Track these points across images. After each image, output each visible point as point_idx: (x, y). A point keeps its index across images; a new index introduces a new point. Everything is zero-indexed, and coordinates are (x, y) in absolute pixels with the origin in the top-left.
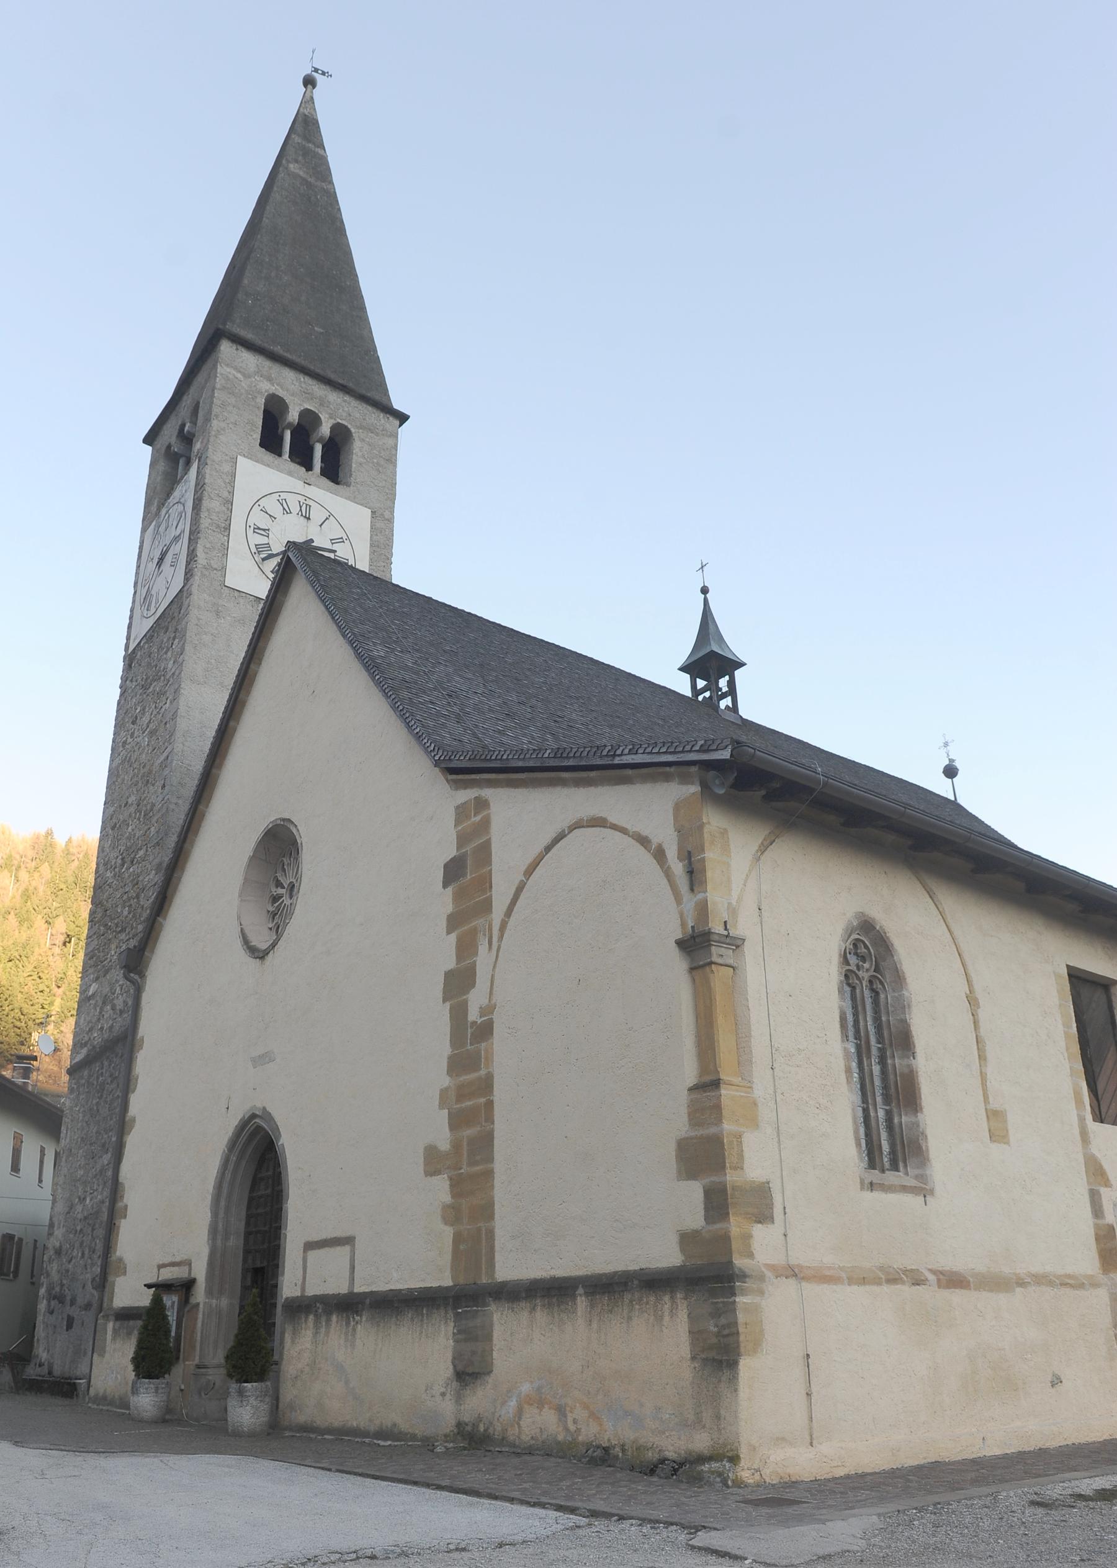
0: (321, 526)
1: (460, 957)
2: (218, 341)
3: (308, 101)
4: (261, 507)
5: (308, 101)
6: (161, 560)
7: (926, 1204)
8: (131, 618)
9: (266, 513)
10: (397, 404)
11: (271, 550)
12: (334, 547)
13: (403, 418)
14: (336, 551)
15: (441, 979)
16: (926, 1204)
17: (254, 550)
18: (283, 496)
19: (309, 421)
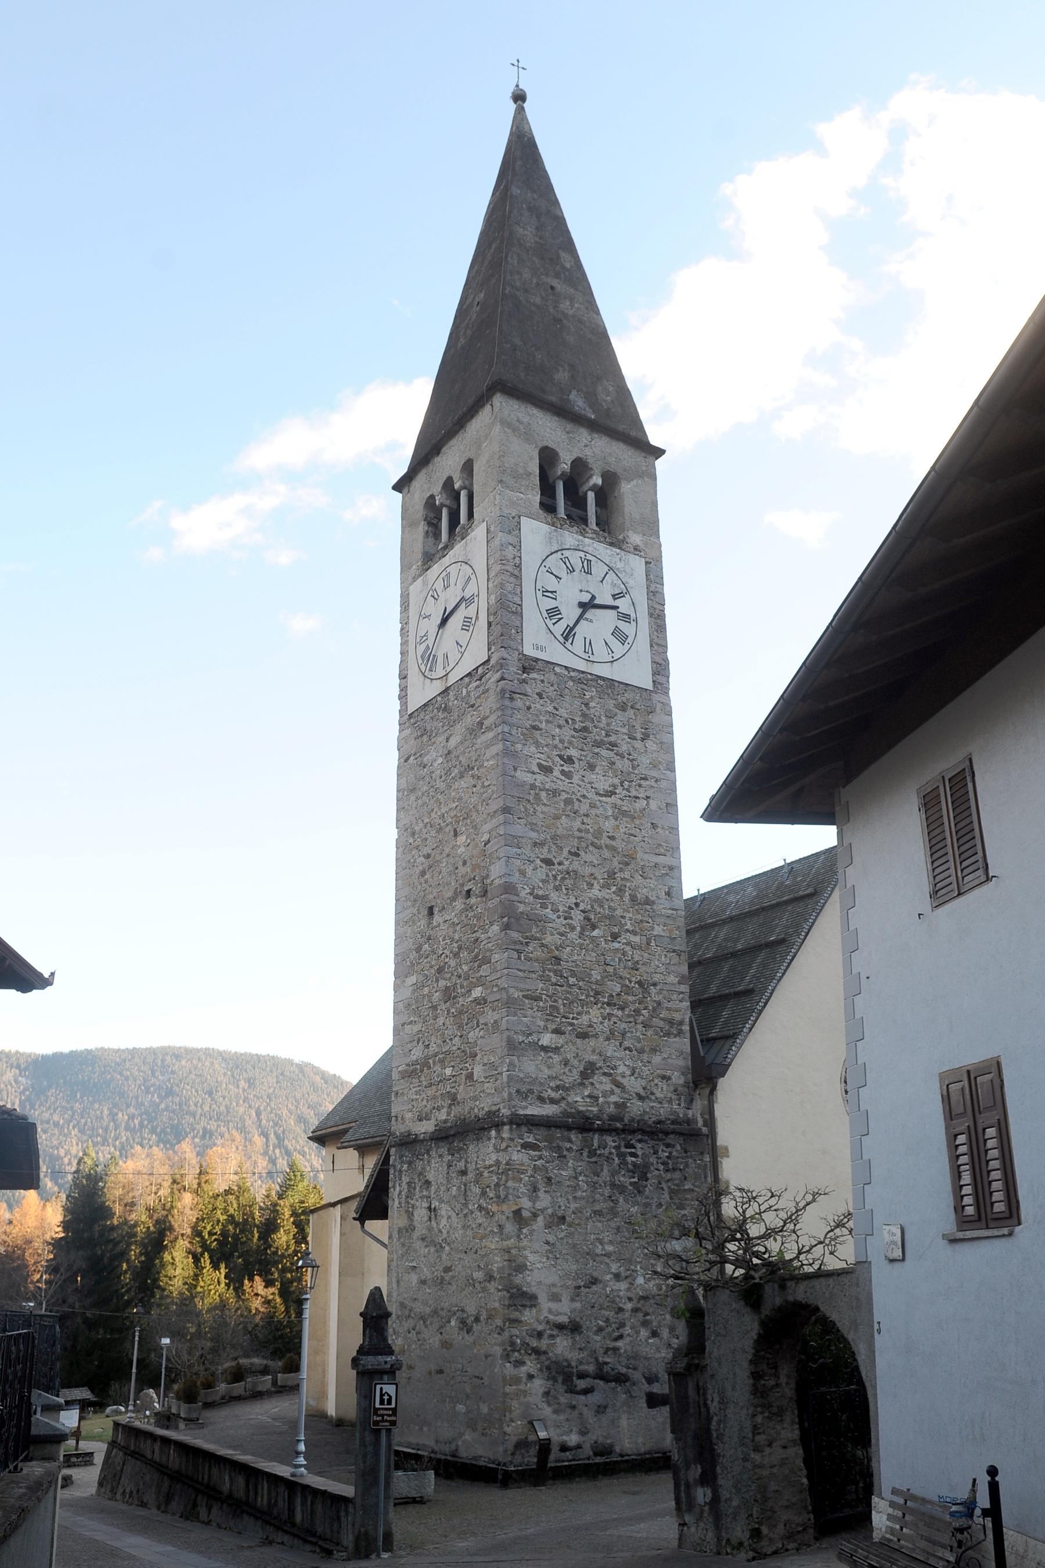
0: (602, 581)
1: (523, 108)
2: (494, 393)
3: (520, 120)
4: (547, 568)
5: (520, 120)
6: (444, 621)
7: (975, 1480)
8: (403, 677)
9: (552, 573)
10: (654, 440)
11: (560, 614)
12: (616, 603)
13: (659, 452)
14: (618, 607)
15: (987, 1484)
16: (975, 1480)
17: (545, 615)
18: (566, 553)
19: (580, 466)
